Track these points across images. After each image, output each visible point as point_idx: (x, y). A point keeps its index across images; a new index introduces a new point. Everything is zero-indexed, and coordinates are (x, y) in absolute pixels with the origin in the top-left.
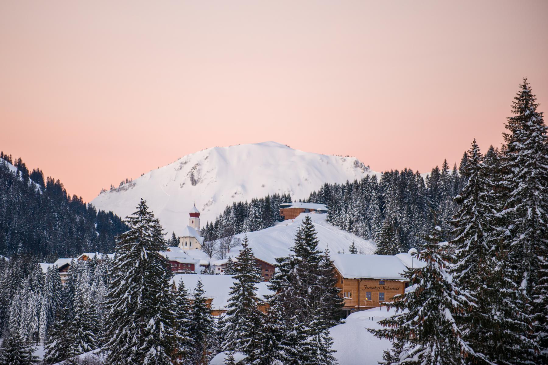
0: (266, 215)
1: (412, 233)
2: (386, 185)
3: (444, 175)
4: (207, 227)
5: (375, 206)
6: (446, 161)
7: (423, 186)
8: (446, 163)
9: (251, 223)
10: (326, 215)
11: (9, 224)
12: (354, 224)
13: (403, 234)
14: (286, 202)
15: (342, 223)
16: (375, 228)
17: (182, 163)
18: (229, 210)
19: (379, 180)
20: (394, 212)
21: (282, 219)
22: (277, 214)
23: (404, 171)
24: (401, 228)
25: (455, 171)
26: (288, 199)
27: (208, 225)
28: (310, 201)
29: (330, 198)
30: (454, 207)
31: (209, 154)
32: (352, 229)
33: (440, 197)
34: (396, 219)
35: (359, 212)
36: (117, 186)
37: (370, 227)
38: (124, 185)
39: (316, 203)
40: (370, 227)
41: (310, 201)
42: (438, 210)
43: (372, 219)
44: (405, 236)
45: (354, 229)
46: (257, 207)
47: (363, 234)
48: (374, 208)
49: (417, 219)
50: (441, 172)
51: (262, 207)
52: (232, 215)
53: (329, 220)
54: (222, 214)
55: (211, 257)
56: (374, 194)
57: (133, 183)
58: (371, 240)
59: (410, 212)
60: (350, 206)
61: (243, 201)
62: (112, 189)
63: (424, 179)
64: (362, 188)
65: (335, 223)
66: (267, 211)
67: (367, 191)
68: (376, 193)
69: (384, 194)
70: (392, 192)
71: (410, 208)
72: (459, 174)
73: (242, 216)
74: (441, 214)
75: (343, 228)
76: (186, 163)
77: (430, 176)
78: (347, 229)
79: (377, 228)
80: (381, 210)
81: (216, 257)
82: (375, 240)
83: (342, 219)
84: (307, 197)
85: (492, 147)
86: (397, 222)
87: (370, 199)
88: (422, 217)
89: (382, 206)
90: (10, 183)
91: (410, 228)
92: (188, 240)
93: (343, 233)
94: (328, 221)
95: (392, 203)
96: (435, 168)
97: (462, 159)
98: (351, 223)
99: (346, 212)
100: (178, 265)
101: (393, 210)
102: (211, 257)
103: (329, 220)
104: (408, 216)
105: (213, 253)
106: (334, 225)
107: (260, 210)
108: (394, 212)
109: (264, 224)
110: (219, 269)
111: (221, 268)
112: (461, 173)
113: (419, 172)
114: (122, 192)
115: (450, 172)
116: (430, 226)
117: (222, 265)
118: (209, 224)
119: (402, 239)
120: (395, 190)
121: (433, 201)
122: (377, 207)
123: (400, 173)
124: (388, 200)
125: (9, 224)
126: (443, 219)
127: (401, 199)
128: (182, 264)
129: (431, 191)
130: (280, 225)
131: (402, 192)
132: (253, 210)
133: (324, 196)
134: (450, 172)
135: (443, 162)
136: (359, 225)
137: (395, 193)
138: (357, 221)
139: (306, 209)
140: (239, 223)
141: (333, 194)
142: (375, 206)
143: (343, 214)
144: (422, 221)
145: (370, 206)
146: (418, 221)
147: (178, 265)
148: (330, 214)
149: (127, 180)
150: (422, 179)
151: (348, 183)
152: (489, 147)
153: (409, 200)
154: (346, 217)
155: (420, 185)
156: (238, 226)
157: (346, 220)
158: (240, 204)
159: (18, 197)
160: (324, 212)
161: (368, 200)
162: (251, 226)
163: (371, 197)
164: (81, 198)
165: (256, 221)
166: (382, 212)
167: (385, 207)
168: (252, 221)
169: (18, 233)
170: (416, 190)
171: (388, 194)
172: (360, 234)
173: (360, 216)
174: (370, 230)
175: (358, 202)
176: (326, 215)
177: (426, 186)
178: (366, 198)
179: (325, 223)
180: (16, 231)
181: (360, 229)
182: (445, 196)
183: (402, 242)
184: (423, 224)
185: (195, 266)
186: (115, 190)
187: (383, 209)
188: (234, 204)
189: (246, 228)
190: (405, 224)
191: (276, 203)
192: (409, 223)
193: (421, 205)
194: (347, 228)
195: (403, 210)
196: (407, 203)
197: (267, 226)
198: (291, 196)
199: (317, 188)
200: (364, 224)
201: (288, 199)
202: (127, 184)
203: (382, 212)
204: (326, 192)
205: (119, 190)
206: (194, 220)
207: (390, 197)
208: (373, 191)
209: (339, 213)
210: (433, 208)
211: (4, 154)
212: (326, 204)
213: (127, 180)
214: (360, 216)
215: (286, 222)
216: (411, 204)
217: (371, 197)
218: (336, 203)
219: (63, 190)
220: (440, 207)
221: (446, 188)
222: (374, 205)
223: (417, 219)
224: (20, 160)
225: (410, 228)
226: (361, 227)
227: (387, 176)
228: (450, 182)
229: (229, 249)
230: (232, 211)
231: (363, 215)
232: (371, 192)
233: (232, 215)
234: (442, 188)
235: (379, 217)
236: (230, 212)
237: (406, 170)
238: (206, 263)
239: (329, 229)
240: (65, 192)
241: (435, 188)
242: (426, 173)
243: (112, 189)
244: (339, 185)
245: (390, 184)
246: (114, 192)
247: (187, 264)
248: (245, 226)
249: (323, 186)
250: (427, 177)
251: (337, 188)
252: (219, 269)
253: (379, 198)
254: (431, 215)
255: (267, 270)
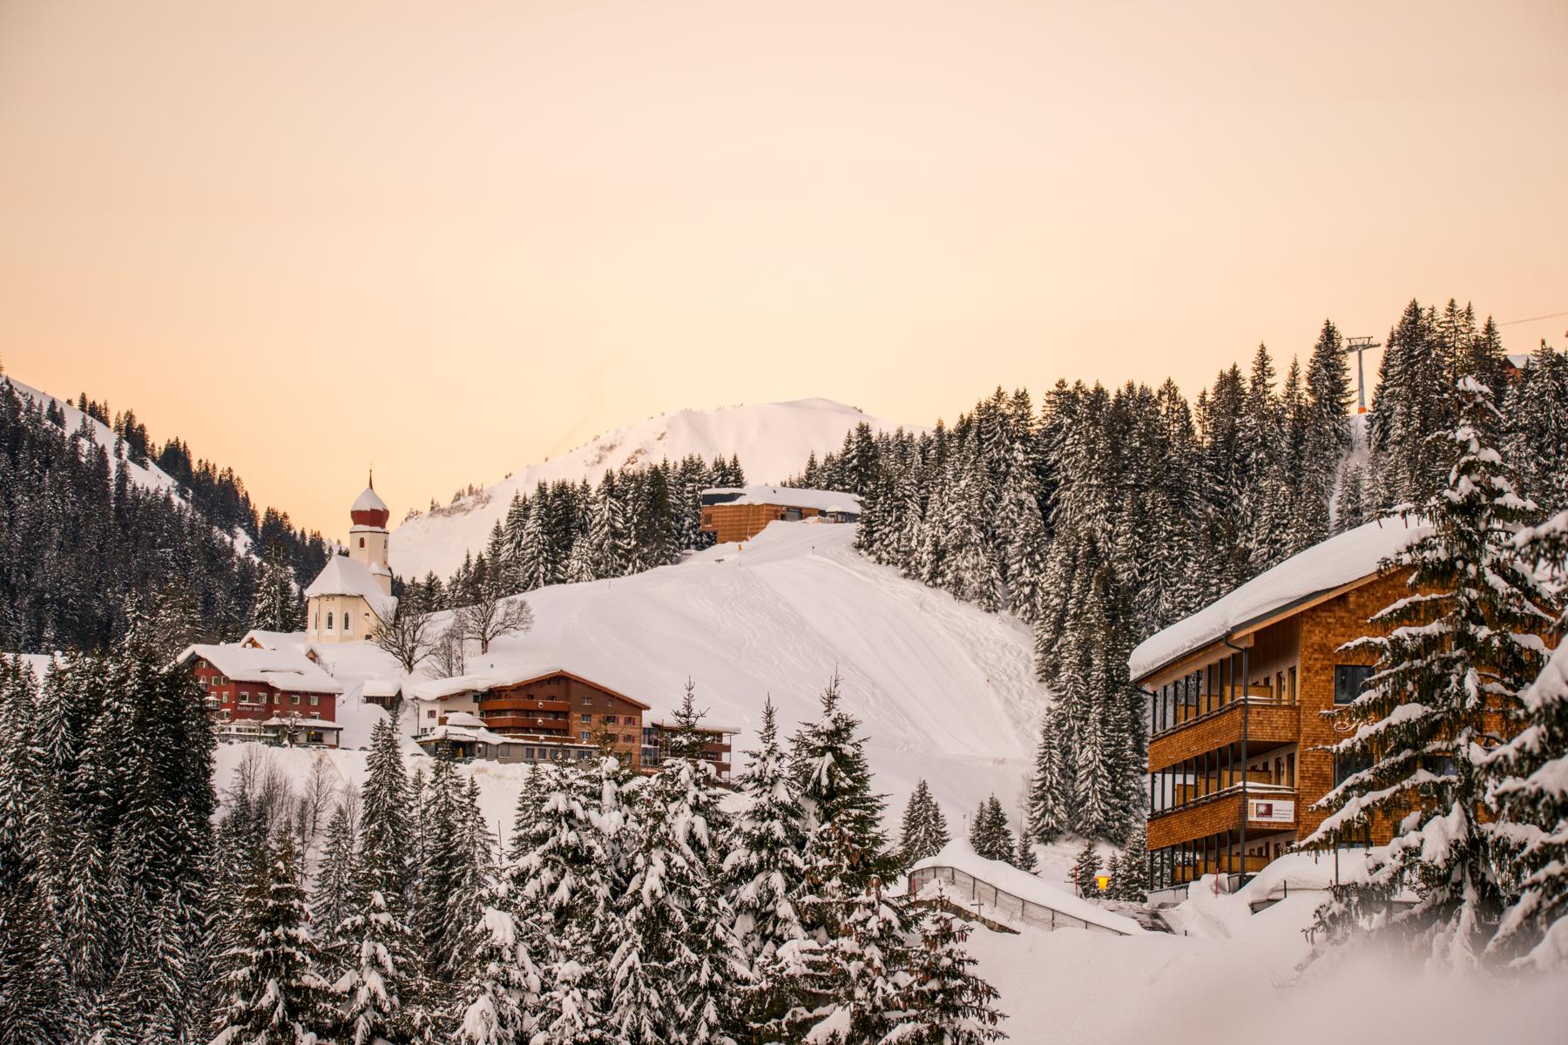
0: (651, 525)
1: (1147, 590)
2: (1060, 426)
3: (1259, 399)
4: (466, 571)
5: (1024, 495)
6: (1263, 349)
7: (1188, 430)
8: (1263, 358)
9: (597, 555)
10: (852, 530)
11: (29, 576)
12: (949, 557)
13: (1117, 591)
14: (723, 484)
15: (910, 553)
16: (1020, 573)
17: (602, 448)
18: (521, 512)
19: (1039, 410)
20: (1089, 517)
21: (707, 540)
22: (692, 527)
23: (1124, 391)
24: (1112, 571)
25: (1293, 384)
26: (730, 474)
27: (468, 564)
28: (808, 482)
29: (873, 479)
30: (1292, 504)
31: (669, 426)
32: (943, 574)
33: (1244, 469)
34: (1092, 541)
35: (968, 517)
36: (445, 502)
37: (1004, 568)
38: (462, 500)
39: (827, 488)
40: (1004, 568)
41: (808, 482)
42: (1236, 512)
43: (1011, 543)
44: (1124, 601)
45: (949, 577)
46: (618, 498)
47: (981, 594)
48: (1020, 504)
49: (1166, 540)
50: (1247, 386)
51: (635, 500)
52: (532, 525)
53: (866, 543)
54: (503, 524)
55: (411, 669)
56: (1021, 457)
57: (485, 495)
58: (1005, 613)
59: (1142, 517)
60: (936, 496)
61: (574, 479)
62: (435, 509)
63: (1191, 406)
64: (978, 434)
65: (885, 556)
66: (654, 514)
67: (997, 444)
68: (1025, 452)
69: (1053, 457)
70: (1082, 449)
71: (1144, 504)
72: (1306, 395)
73: (567, 531)
74: (1249, 527)
75: (912, 573)
76: (612, 447)
77: (1209, 398)
78: (926, 576)
79: (1027, 572)
80: (1045, 510)
81: (427, 669)
82: (1019, 615)
83: (910, 540)
84: (799, 470)
85: (1414, 304)
86: (1094, 551)
87: (1006, 474)
88: (1182, 534)
89: (1046, 497)
90: (47, 463)
91: (1142, 572)
92: (336, 608)
93: (913, 588)
94: (859, 546)
95: (1081, 488)
96: (1227, 371)
97: (1318, 347)
98: (940, 554)
99: (922, 518)
100: (270, 699)
101: (1084, 508)
102: (411, 669)
103: (866, 543)
104: (1134, 532)
105: (418, 654)
106: (880, 560)
107: (629, 509)
108: (1089, 517)
109: (643, 558)
110: (432, 714)
111: (437, 708)
112: (1313, 392)
113: (1176, 384)
114: (459, 516)
115: (1278, 388)
116: (1209, 566)
117: (443, 699)
118: (474, 561)
119: (1114, 608)
120: (1093, 441)
121: (1220, 483)
122: (1031, 501)
123: (1112, 397)
124: (1066, 478)
125: (29, 576)
126: (1251, 545)
127: (1113, 472)
128: (288, 694)
129: (1213, 447)
130: (697, 562)
131: (1115, 448)
132: (602, 510)
133: (855, 468)
134: (1278, 388)
135: (1253, 355)
136: (964, 562)
137: (1091, 452)
138: (958, 548)
139: (789, 508)
140: (555, 554)
141: (889, 462)
142: (1024, 495)
143: (914, 526)
144: (1181, 547)
145: (1006, 497)
146: (1171, 548)
147: (270, 699)
148: (869, 522)
149: (471, 488)
150: (1184, 405)
151: (940, 429)
152: (1406, 305)
153: (1140, 478)
154: (922, 532)
155: (1176, 428)
156: (554, 562)
157: (921, 543)
158: (562, 489)
159: (58, 502)
160: (849, 517)
161: (997, 474)
162: (598, 563)
163: (1009, 466)
164: (285, 516)
165: (614, 548)
166: (1045, 517)
167: (1056, 501)
168: (600, 546)
169: (52, 600)
170: (1165, 444)
171: (1068, 456)
172: (969, 593)
173: (968, 532)
174: (1005, 581)
175: (963, 484)
176: (852, 530)
177: (1198, 432)
178: (993, 471)
179: (850, 554)
180: (47, 596)
181: (968, 575)
182: (1260, 464)
183: (1114, 618)
184: (1186, 558)
185: (339, 700)
186: (443, 511)
187: (1050, 509)
188: (542, 489)
189: (581, 570)
190: (1124, 559)
191: (689, 487)
192: (1139, 556)
193: (1178, 495)
194: (925, 571)
195: (1120, 509)
196: (1133, 487)
197: (649, 562)
198: (742, 465)
199: (832, 443)
200: (983, 560)
201: (730, 474)
202: (471, 499)
203: (1045, 517)
204: (862, 453)
205: (449, 512)
206: (367, 537)
207: (1075, 467)
208: (1017, 445)
209: (898, 519)
210: (1221, 505)
211: (90, 400)
212: (862, 494)
213: (471, 488)
214: (968, 532)
215: (717, 550)
216: (1146, 489)
217: (1009, 466)
218: (890, 486)
219: (242, 494)
220: (1245, 501)
221: (1264, 438)
222: (1020, 493)
223: (1166, 540)
224: (130, 417)
225: (1142, 572)
226: (975, 567)
227: (1066, 400)
228: (1279, 421)
229: (485, 643)
230: (533, 512)
231: (982, 528)
232: (1010, 450)
233: (532, 525)
234: (1252, 439)
235: (1036, 536)
236: (527, 517)
237: (1131, 388)
238: (390, 692)
239: (864, 573)
240: (247, 500)
241: (1228, 440)
242: (1196, 386)
243: (435, 509)
244: (911, 436)
245: (1076, 422)
246: (440, 518)
247: (306, 695)
248: (575, 564)
249: (854, 433)
250: (1203, 402)
251: (903, 445)
252: (432, 714)
253: (1039, 471)
254: (1213, 528)
255: (609, 719)
